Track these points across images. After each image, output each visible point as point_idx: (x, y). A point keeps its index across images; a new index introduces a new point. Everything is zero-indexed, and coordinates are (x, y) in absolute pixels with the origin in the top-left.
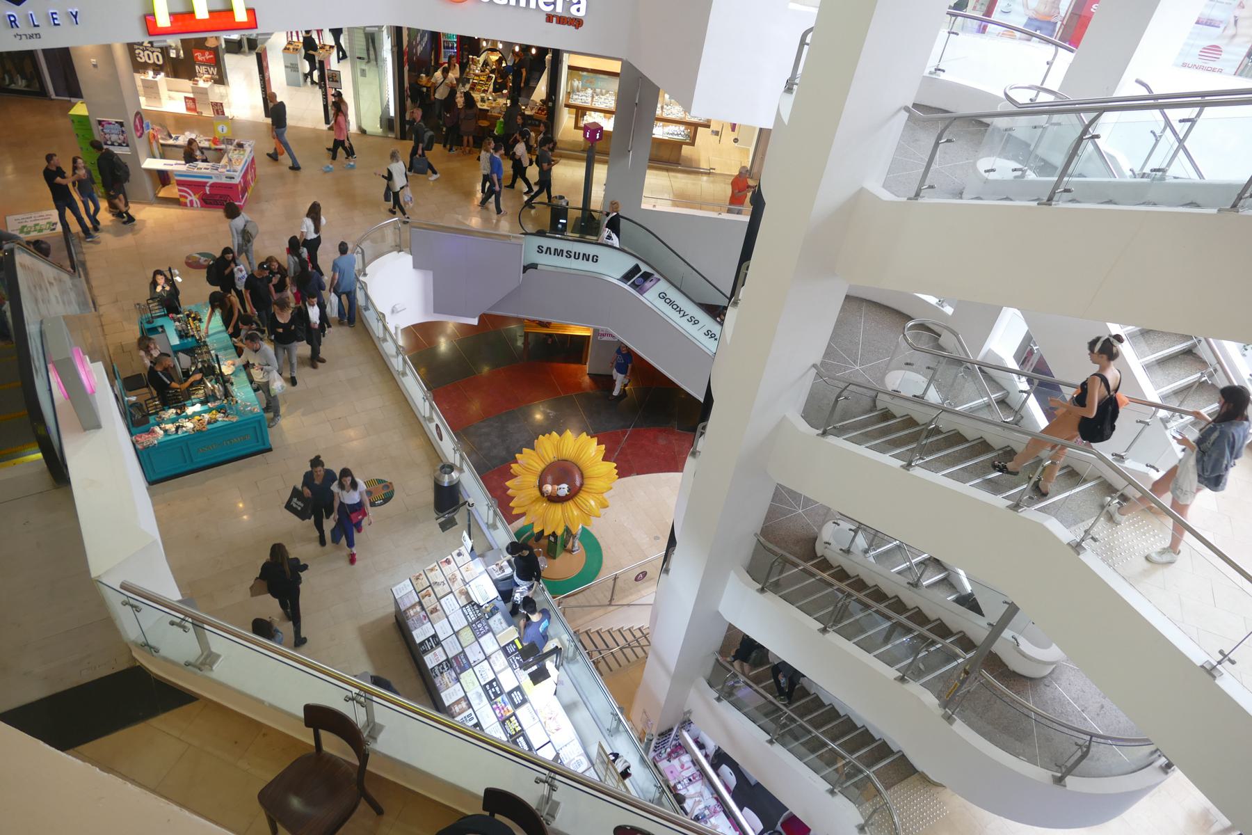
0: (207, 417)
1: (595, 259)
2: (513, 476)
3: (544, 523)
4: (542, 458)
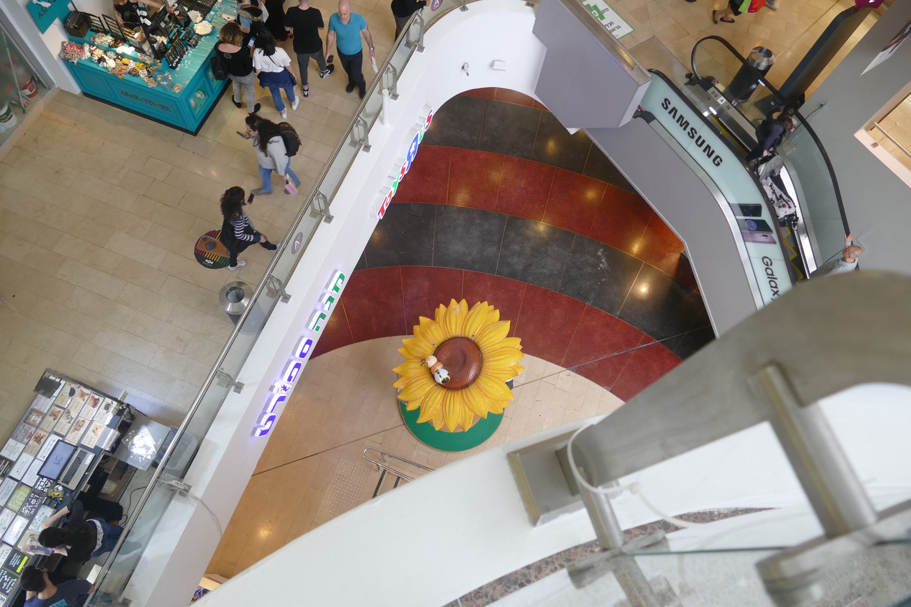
0: (132, 64)
1: (718, 161)
2: (432, 317)
3: (408, 386)
4: (464, 326)
